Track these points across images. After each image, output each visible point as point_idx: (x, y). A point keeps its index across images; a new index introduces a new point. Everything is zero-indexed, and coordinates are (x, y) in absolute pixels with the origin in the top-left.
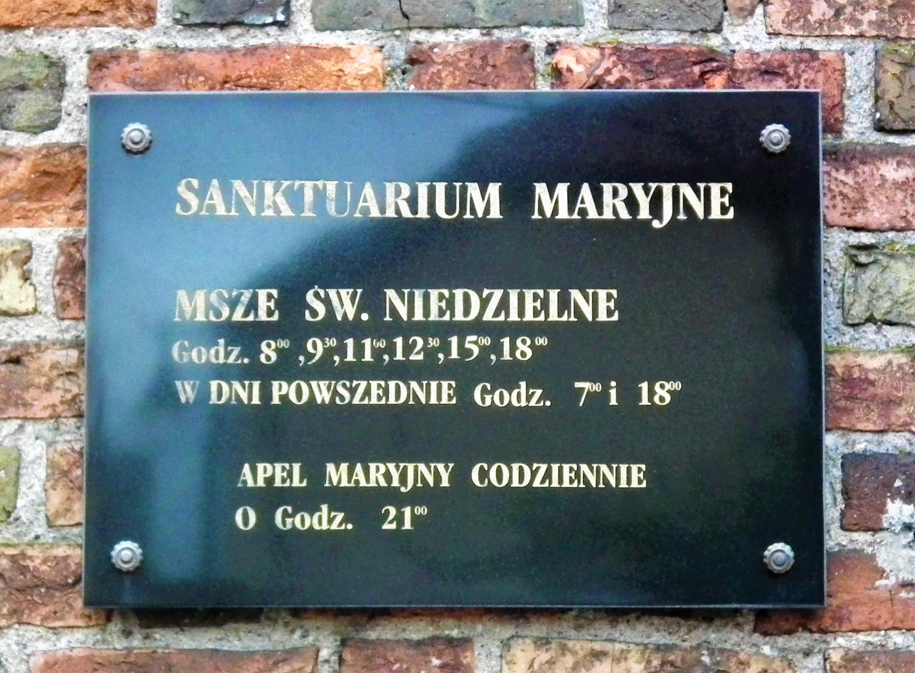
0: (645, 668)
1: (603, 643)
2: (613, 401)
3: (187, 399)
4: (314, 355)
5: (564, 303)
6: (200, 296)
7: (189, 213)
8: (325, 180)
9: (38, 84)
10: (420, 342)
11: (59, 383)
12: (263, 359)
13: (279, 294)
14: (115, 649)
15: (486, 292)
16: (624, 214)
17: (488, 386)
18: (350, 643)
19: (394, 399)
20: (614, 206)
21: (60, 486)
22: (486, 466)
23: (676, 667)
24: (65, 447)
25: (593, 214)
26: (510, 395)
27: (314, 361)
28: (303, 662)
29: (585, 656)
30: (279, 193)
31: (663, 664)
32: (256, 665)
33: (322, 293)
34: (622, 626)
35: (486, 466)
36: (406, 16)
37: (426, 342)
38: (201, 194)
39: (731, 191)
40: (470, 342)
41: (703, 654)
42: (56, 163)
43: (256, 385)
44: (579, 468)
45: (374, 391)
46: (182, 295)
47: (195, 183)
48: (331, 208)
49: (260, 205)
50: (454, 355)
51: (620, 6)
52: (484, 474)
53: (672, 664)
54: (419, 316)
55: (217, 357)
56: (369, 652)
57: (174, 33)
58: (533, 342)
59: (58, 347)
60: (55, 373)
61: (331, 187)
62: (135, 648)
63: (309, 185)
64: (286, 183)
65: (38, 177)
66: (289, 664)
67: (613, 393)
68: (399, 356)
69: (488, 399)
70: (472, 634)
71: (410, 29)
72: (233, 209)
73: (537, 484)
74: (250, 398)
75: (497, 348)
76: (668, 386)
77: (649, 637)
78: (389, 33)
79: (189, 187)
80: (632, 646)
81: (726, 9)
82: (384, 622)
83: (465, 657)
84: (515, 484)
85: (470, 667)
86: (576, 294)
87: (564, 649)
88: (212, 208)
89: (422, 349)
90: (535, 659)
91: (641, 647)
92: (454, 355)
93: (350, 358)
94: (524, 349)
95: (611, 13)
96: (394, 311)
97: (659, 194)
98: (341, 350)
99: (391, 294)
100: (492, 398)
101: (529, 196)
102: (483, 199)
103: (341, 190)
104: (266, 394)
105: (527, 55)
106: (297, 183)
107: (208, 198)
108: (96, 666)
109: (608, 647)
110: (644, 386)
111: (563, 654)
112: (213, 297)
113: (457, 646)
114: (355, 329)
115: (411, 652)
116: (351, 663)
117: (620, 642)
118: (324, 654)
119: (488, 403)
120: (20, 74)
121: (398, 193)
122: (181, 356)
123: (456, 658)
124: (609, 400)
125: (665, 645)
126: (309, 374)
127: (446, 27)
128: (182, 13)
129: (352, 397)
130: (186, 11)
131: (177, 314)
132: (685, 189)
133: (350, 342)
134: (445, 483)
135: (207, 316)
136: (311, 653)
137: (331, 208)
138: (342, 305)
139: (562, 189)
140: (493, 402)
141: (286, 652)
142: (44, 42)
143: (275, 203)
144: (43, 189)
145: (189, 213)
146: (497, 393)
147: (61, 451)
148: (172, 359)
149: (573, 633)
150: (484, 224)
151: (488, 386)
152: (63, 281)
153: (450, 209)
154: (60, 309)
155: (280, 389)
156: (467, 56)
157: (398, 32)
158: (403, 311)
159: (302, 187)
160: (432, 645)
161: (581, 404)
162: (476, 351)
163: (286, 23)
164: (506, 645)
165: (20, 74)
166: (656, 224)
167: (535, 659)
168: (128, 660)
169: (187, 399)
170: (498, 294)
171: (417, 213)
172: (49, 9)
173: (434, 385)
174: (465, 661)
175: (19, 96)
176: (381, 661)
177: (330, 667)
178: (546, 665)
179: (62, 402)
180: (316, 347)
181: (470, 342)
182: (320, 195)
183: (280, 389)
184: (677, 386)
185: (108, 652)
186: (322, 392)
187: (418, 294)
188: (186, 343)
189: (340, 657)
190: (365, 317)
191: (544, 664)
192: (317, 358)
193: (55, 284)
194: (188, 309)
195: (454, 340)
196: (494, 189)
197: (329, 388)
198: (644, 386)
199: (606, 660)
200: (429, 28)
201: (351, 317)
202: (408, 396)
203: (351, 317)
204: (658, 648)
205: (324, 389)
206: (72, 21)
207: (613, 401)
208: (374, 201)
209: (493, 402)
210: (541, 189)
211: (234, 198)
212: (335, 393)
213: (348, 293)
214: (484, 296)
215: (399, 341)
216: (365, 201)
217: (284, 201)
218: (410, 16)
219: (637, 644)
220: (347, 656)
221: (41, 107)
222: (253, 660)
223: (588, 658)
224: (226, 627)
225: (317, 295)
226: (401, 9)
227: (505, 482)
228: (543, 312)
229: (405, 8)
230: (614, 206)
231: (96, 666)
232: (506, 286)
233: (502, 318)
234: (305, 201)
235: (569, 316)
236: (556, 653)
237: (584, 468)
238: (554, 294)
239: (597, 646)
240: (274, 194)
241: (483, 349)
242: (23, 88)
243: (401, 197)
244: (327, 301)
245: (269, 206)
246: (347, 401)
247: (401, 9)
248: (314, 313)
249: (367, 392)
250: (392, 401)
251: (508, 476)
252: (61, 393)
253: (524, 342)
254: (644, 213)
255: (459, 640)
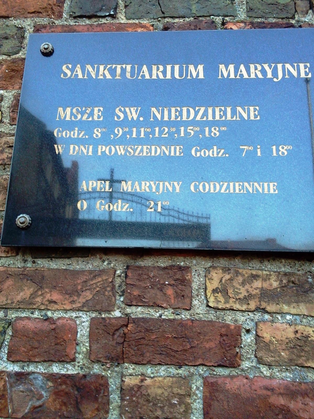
0: (280, 284)
1: (257, 271)
2: (259, 154)
3: (59, 153)
4: (118, 135)
5: (234, 113)
6: (68, 110)
7: (67, 77)
8: (126, 65)
9: (13, 36)
10: (166, 130)
11: (7, 150)
12: (94, 136)
13: (103, 110)
14: (18, 268)
15: (197, 108)
16: (260, 76)
17: (199, 148)
18: (130, 267)
19: (154, 154)
20: (255, 73)
21: (2, 193)
22: (197, 183)
23: (295, 284)
24: (7, 177)
25: (246, 76)
26: (209, 152)
27: (118, 137)
28: (108, 276)
29: (248, 277)
30: (106, 70)
31: (289, 281)
32: (85, 277)
33: (123, 109)
34: (266, 263)
35: (197, 183)
36: (163, 13)
37: (169, 129)
38: (72, 70)
39: (309, 67)
40: (189, 129)
41: (309, 278)
42: (17, 65)
43: (91, 148)
44: (243, 184)
45: (145, 150)
46: (60, 109)
47: (70, 66)
48: (128, 75)
49: (97, 74)
50: (182, 135)
51: (252, 9)
52: (196, 187)
53: (293, 282)
54: (166, 118)
55: (74, 135)
56: (140, 272)
57: (70, 21)
58: (219, 129)
59: (8, 135)
60: (6, 146)
61: (129, 67)
62: (28, 267)
63: (119, 67)
64: (109, 66)
65: (9, 72)
66: (101, 277)
67: (259, 150)
68: (157, 135)
69: (198, 154)
70: (190, 265)
71: (165, 17)
72: (86, 76)
73: (222, 191)
74: (88, 153)
75: (203, 132)
76: (285, 148)
77: (280, 268)
78: (156, 20)
79: (68, 68)
80: (272, 273)
81: (296, 11)
82: (147, 258)
83: (187, 276)
84: (212, 191)
85: (190, 281)
86: (239, 109)
87: (237, 273)
88: (77, 75)
89: (167, 133)
90: (222, 277)
91: (277, 274)
92: (182, 135)
93: (134, 136)
94: (215, 132)
95: (248, 12)
96: (155, 116)
97: (276, 68)
98: (131, 133)
99: (154, 109)
100: (200, 153)
101: (217, 69)
102: (196, 71)
103: (133, 68)
104: (95, 151)
105: (214, 24)
106: (114, 66)
107: (75, 72)
108: (8, 276)
109: (260, 272)
110: (274, 148)
111: (237, 276)
112: (74, 110)
113: (183, 270)
114: (136, 124)
115: (161, 272)
116: (131, 277)
117: (266, 271)
118: (118, 272)
119: (198, 154)
120: (6, 33)
121: (158, 69)
122: (58, 135)
123: (183, 276)
124: (257, 153)
125: (289, 273)
126: (115, 143)
127: (179, 17)
128: (73, 12)
129: (134, 153)
130: (74, 11)
131: (58, 117)
132: (288, 66)
133: (135, 130)
134: (178, 191)
135: (71, 118)
136: (112, 272)
137: (128, 75)
138: (131, 114)
139: (231, 67)
140: (201, 155)
141: (100, 271)
142: (17, 22)
143: (104, 73)
144: (11, 77)
145: (67, 77)
146: (203, 151)
147: (5, 179)
148: (54, 135)
149: (241, 266)
150: (197, 81)
151: (199, 148)
152: (14, 110)
153: (181, 75)
154: (11, 120)
155: (102, 149)
156: (188, 25)
157: (160, 19)
158: (159, 117)
159: (116, 67)
160: (171, 269)
161: (243, 155)
162: (192, 133)
163: (115, 16)
164: (208, 271)
165: (6, 33)
166: (275, 80)
167: (222, 277)
168: (24, 273)
169: (59, 153)
170: (203, 109)
171: (166, 77)
172: (20, 11)
173: (173, 148)
174: (187, 278)
175: (5, 41)
176: (146, 277)
177: (121, 279)
178: (229, 281)
179: (7, 158)
180: (119, 132)
181: (189, 129)
182: (124, 71)
183: (102, 149)
184: (290, 147)
185: (15, 269)
186: (121, 151)
187: (173, 148)
188: (61, 129)
189: (126, 274)
190: (141, 119)
191: (227, 280)
192: (119, 136)
193: (11, 111)
194: (63, 116)
195: (182, 129)
196: (200, 67)
197: (124, 149)
198: (274, 148)
199: (259, 280)
200: (173, 17)
201: (135, 119)
202: (161, 152)
203: (135, 119)
204: (286, 274)
205: (122, 149)
206: (29, 15)
207: (259, 154)
208: (147, 72)
209: (201, 155)
210: (222, 67)
211: (86, 71)
212: (127, 151)
213: (134, 109)
214: (196, 110)
215: (157, 129)
216: (143, 72)
217: (108, 73)
218: (165, 13)
219: (275, 272)
220: (129, 274)
221: (13, 45)
222: (84, 275)
223: (250, 278)
224: (72, 259)
225: (120, 110)
226: (161, 10)
227: (207, 190)
228: (224, 116)
229: (162, 10)
230: (255, 73)
231: (8, 276)
232: (207, 106)
233: (205, 119)
234: (117, 72)
235: (236, 118)
236: (234, 275)
237: (246, 184)
238: (229, 110)
239: (254, 273)
240: (104, 70)
241: (196, 132)
242: (6, 38)
243: (160, 71)
244: (125, 113)
245: (101, 75)
246: (132, 154)
247: (161, 10)
248: (119, 117)
249: (142, 151)
250: (153, 154)
251: (208, 188)
252: (7, 154)
253: (215, 129)
254: (269, 75)
255: (184, 267)
